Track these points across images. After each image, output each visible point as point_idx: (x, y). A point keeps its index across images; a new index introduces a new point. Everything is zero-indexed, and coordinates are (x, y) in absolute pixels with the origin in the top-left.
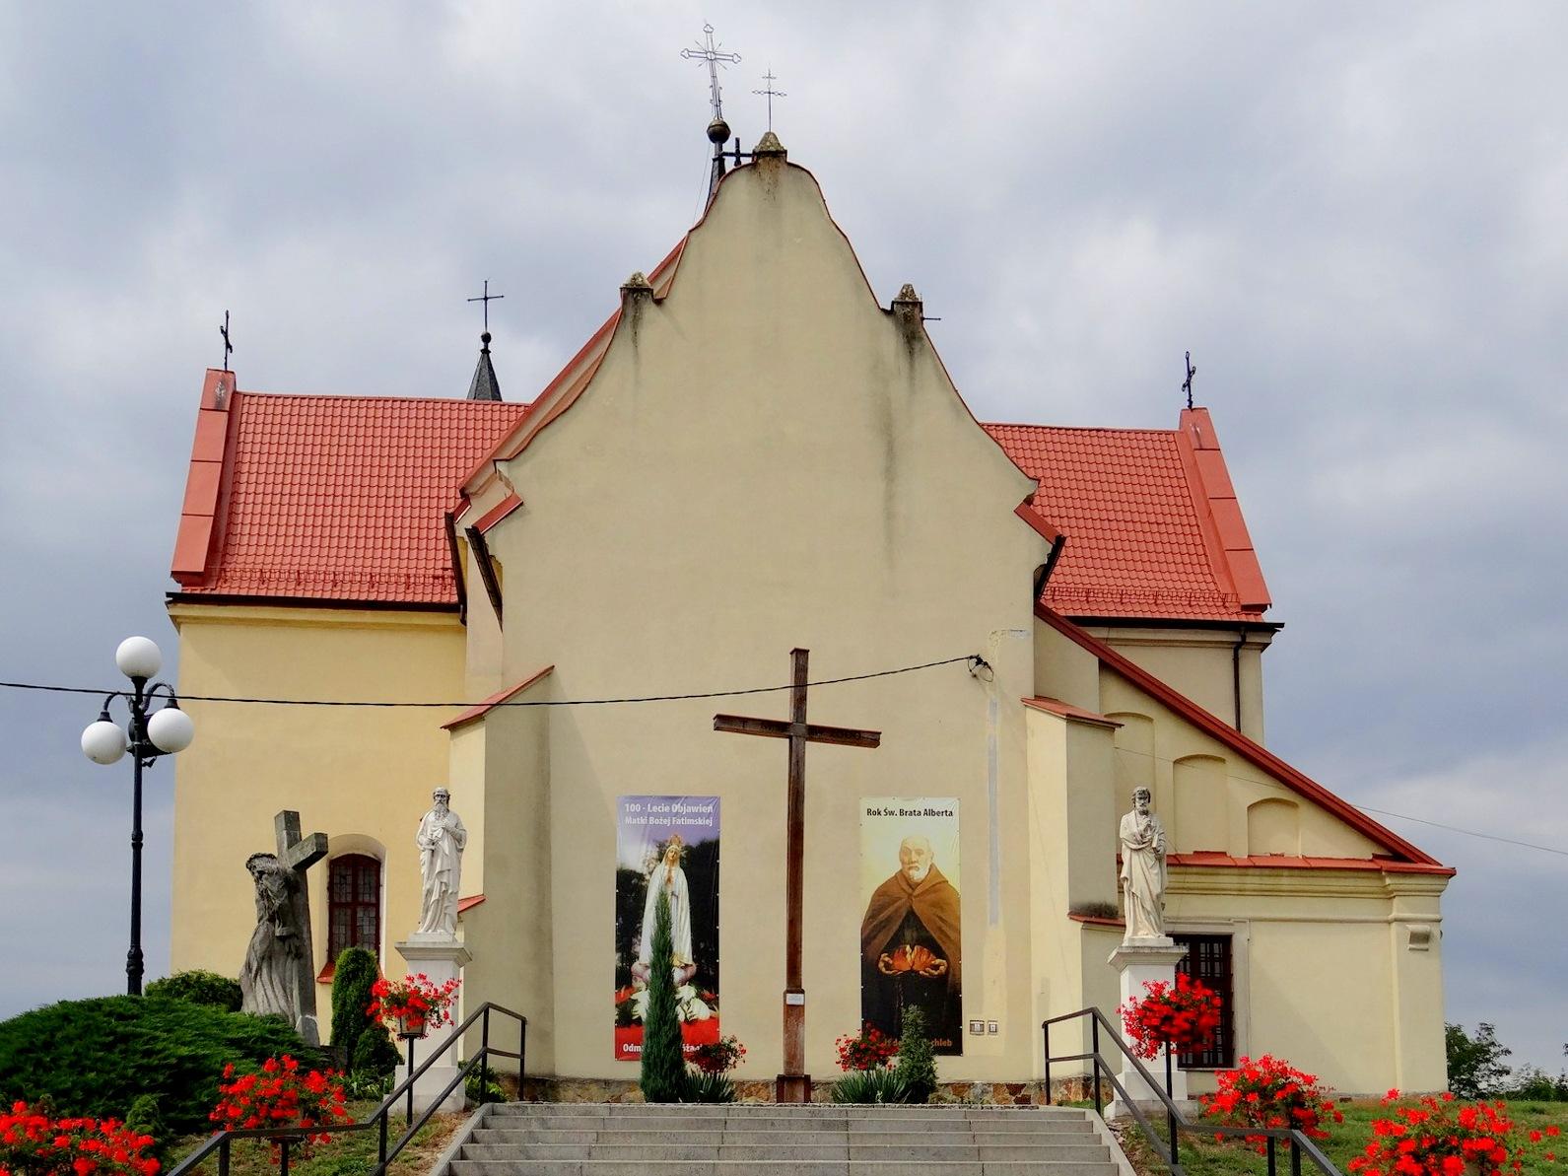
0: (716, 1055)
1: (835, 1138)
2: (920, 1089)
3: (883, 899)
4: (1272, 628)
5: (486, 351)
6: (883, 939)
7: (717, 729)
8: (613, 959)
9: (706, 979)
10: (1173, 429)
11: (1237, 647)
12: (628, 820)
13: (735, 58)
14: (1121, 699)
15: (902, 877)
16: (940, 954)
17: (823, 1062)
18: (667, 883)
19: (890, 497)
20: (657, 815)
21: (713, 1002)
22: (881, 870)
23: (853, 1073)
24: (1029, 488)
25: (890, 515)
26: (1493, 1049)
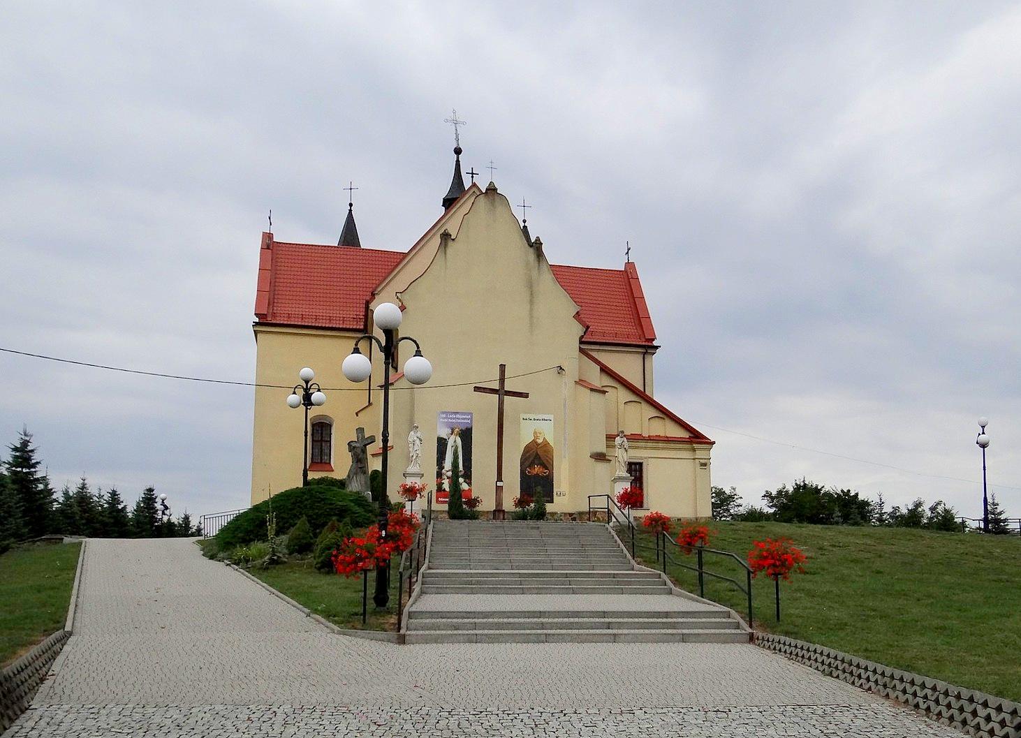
0: (473, 502)
1: (535, 532)
2: (540, 515)
3: (528, 449)
4: (657, 347)
5: (350, 210)
6: (527, 463)
7: (475, 391)
8: (435, 468)
9: (468, 476)
10: (621, 269)
11: (644, 354)
12: (442, 420)
13: (464, 123)
14: (607, 381)
15: (534, 441)
16: (545, 467)
17: (509, 505)
18: (454, 442)
19: (531, 310)
20: (451, 418)
21: (469, 484)
22: (527, 439)
23: (518, 509)
24: (578, 308)
25: (531, 317)
26: (735, 497)
